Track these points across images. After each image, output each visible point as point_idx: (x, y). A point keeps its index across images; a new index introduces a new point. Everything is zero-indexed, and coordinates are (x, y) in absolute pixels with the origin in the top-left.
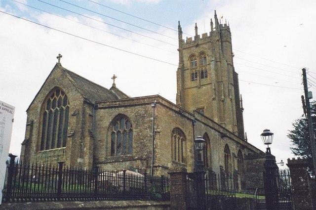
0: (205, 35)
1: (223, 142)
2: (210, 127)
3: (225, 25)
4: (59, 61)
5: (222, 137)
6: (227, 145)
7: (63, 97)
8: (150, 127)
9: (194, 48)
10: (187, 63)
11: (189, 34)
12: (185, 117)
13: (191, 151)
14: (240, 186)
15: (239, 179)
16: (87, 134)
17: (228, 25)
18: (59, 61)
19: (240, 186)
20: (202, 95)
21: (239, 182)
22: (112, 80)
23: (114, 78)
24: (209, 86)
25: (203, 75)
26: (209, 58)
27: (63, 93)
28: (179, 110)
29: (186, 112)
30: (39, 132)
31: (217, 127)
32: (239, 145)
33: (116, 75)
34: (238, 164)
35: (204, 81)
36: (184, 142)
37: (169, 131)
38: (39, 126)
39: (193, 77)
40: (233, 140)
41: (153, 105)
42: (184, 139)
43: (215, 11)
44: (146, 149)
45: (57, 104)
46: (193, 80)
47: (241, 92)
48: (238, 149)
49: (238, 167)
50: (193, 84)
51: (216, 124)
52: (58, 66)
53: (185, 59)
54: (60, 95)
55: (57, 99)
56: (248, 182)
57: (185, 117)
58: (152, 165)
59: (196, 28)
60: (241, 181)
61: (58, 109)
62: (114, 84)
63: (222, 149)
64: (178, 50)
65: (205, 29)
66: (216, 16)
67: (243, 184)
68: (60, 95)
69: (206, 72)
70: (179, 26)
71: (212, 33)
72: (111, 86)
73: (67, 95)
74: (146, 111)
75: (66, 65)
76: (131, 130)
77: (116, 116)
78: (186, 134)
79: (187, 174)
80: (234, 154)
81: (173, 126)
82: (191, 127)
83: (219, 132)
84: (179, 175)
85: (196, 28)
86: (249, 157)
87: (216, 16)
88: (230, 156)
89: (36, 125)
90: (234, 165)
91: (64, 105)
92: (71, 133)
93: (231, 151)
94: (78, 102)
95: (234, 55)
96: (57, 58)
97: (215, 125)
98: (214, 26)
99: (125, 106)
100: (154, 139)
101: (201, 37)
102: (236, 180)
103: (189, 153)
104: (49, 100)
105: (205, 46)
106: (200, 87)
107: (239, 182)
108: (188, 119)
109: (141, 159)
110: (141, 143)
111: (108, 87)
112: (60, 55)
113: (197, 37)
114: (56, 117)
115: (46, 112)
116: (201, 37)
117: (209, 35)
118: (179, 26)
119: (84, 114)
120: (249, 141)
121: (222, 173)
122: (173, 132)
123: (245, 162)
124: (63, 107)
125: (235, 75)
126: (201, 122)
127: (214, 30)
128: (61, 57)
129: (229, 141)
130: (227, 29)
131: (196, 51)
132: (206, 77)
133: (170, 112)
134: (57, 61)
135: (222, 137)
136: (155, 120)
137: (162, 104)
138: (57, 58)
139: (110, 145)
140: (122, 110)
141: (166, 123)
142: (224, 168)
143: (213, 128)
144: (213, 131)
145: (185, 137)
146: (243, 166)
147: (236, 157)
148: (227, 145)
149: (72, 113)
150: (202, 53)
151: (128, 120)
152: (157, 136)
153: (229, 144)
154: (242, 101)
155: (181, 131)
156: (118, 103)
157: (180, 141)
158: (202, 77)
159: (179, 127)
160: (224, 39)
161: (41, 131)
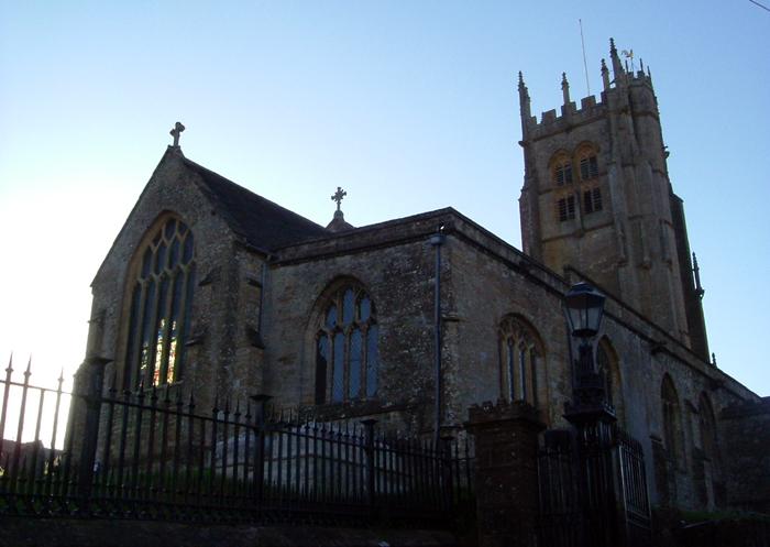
0: (549, 116)
1: (656, 367)
2: (618, 321)
3: (641, 73)
4: (176, 141)
5: (654, 353)
6: (667, 376)
7: (182, 239)
8: (428, 309)
9: (562, 136)
10: (546, 176)
11: (546, 102)
12: (540, 283)
13: (561, 388)
14: (711, 495)
15: (708, 475)
16: (240, 337)
17: (647, 74)
18: (176, 141)
19: (711, 495)
20: (584, 250)
21: (709, 485)
22: (335, 203)
23: (339, 196)
24: (608, 230)
25: (592, 202)
26: (600, 158)
27: (183, 227)
28: (523, 265)
29: (542, 268)
30: (118, 342)
31: (637, 323)
32: (702, 379)
33: (344, 189)
34: (702, 433)
36: (539, 361)
38: (120, 322)
39: (564, 211)
40: (686, 363)
41: (435, 239)
42: (540, 351)
43: (612, 40)
44: (416, 378)
45: (166, 259)
46: (563, 218)
47: (693, 247)
48: (701, 388)
49: (702, 439)
50: (566, 229)
51: (637, 314)
52: (173, 153)
53: (540, 165)
54: (177, 233)
55: (169, 244)
57: (540, 283)
58: (435, 426)
59: (565, 85)
60: (714, 483)
61: (169, 272)
62: (339, 214)
63: (656, 386)
64: (520, 143)
65: (589, 86)
66: (614, 52)
67: (720, 490)
68: (177, 233)
69: (597, 192)
71: (604, 95)
72: (331, 218)
73: (193, 229)
74: (415, 260)
75: (195, 151)
76: (373, 322)
77: (330, 283)
78: (547, 334)
79: (542, 427)
80: (688, 403)
81: (503, 307)
82: (558, 317)
83: (643, 337)
84: (513, 424)
85: (565, 85)
87: (614, 52)
88: (678, 407)
89: (109, 322)
90: (692, 433)
91: (185, 262)
92: (197, 335)
93: (682, 396)
94: (218, 247)
95: (668, 153)
96: (173, 133)
97: (632, 315)
98: (611, 77)
100: (441, 343)
101: (579, 107)
102: (699, 476)
103: (556, 394)
104: (149, 251)
105: (590, 128)
106: (580, 234)
107: (709, 485)
108: (549, 289)
109: (401, 407)
110: (402, 357)
111: (322, 217)
112: (178, 124)
113: (568, 107)
114: (162, 294)
115: (139, 285)
116: (579, 107)
117: (599, 100)
119: (234, 282)
120: (719, 366)
121: (656, 447)
122: (504, 324)
124: (182, 266)
125: (676, 205)
127: (613, 86)
129: (674, 365)
130: (644, 81)
131: (561, 140)
132: (599, 207)
133: (492, 265)
136: (443, 284)
137: (463, 237)
138: (173, 133)
139: (311, 372)
140: (345, 263)
141: (476, 299)
142: (663, 443)
143: (625, 325)
144: (625, 332)
145: (542, 342)
146: (716, 439)
147: (695, 412)
148: (667, 376)
149: (203, 278)
150: (585, 145)
151: (363, 294)
152: (451, 332)
153: (674, 376)
154: (696, 269)
155: (530, 324)
156: (333, 243)
157: (528, 354)
158: (588, 209)
159: (523, 311)
160: (639, 108)
161: (125, 340)
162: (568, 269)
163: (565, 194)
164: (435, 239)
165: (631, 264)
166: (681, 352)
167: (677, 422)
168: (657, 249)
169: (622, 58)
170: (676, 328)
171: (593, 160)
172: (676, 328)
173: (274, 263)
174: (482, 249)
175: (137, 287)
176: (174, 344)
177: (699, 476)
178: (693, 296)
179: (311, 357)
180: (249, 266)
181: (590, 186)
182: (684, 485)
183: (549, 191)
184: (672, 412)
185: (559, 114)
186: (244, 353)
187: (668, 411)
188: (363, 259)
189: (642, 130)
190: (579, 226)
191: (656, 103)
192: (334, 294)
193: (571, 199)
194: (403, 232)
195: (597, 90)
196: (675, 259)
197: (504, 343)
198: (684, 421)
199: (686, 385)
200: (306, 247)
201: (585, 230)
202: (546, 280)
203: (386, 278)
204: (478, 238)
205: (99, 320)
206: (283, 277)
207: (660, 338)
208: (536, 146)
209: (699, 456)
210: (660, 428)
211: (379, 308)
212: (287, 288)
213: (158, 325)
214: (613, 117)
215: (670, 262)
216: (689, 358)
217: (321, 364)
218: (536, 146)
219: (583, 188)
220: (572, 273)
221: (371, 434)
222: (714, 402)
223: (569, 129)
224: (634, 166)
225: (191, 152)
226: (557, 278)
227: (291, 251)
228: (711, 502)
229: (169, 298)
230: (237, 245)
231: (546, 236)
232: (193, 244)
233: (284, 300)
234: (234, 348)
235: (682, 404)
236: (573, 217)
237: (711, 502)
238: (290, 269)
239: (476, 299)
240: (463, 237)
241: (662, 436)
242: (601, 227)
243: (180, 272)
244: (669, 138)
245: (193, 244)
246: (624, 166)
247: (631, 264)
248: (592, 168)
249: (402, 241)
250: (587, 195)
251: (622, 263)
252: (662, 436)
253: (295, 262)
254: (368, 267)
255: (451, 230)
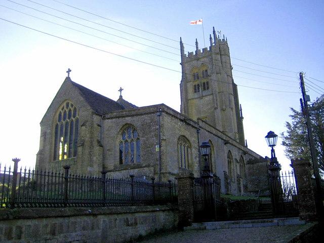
1: (226, 148)
3: (223, 40)
4: (69, 75)
10: (190, 77)
11: (190, 49)
15: (242, 183)
16: (95, 143)
18: (69, 75)
20: (202, 106)
21: (242, 186)
23: (121, 90)
24: (211, 97)
25: (206, 86)
28: (183, 118)
29: (191, 120)
31: (220, 134)
32: (241, 151)
35: (205, 93)
36: (189, 149)
37: (176, 140)
39: (196, 89)
41: (158, 114)
42: (190, 147)
46: (195, 92)
47: (240, 102)
48: (240, 154)
49: (240, 171)
50: (196, 95)
52: (68, 79)
56: (249, 186)
62: (121, 97)
63: (226, 155)
65: (205, 44)
66: (214, 32)
67: (246, 187)
69: (207, 83)
70: (181, 42)
71: (210, 48)
78: (191, 142)
80: (236, 159)
85: (197, 43)
86: (250, 162)
87: (214, 32)
89: (48, 136)
90: (237, 169)
91: (74, 117)
93: (234, 157)
96: (67, 72)
98: (213, 41)
99: (133, 116)
106: (201, 97)
107: (242, 186)
108: (193, 126)
111: (115, 98)
112: (69, 69)
115: (57, 124)
116: (202, 52)
118: (181, 42)
123: (247, 166)
125: (235, 86)
126: (206, 130)
127: (214, 44)
128: (70, 71)
132: (208, 88)
134: (66, 75)
135: (225, 144)
137: (167, 113)
138: (67, 72)
139: (118, 154)
140: (128, 120)
154: (241, 110)
157: (186, 148)
158: (204, 89)
162: (198, 119)
163: (196, 83)
164: (158, 114)
165: (219, 108)
166: (234, 143)
167: (232, 166)
168: (228, 103)
169: (217, 34)
170: (234, 131)
171: (206, 71)
172: (234, 131)
173: (104, 119)
174: (173, 116)
175: (57, 125)
176: (66, 145)
177: (239, 181)
178: (240, 119)
179: (118, 150)
180: (96, 119)
181: (205, 81)
182: (234, 187)
183: (190, 81)
184: (231, 163)
185: (194, 54)
186: (97, 149)
187: (229, 162)
188: (135, 118)
189: (224, 60)
190: (201, 95)
191: (229, 49)
192: (125, 129)
193: (198, 85)
194: (148, 111)
195: (208, 46)
196: (234, 107)
197: (179, 145)
198: (235, 166)
199: (236, 154)
200: (115, 114)
201: (203, 96)
202: (192, 124)
203: (143, 125)
204: (171, 113)
205: (44, 135)
206: (108, 123)
207: (227, 139)
208: (186, 65)
209: (239, 177)
210: (227, 168)
211: (141, 135)
212: (109, 127)
213: (60, 139)
214: (213, 56)
215: (232, 109)
216: (237, 145)
217: (121, 152)
218: (186, 65)
219: (203, 81)
220: (199, 120)
221: (67, 172)
222: (244, 158)
223: (198, 59)
224: (220, 73)
225: (75, 79)
226: (195, 123)
227: (110, 114)
228: (242, 191)
229: (74, 128)
230: (93, 113)
231: (189, 98)
232: (77, 112)
233: (108, 130)
234: (93, 147)
235: (234, 160)
236: (199, 91)
237: (242, 191)
238: (110, 120)
239: (172, 129)
240: (167, 113)
241: (227, 171)
242: (209, 95)
243: (69, 118)
244: (233, 62)
245: (77, 112)
246: (217, 74)
247: (219, 108)
248: (206, 74)
249: (148, 114)
250: (204, 83)
251: (216, 109)
252: (227, 171)
253: (112, 118)
254: (136, 121)
255: (163, 111)
